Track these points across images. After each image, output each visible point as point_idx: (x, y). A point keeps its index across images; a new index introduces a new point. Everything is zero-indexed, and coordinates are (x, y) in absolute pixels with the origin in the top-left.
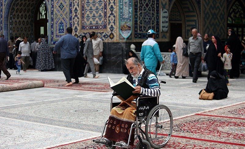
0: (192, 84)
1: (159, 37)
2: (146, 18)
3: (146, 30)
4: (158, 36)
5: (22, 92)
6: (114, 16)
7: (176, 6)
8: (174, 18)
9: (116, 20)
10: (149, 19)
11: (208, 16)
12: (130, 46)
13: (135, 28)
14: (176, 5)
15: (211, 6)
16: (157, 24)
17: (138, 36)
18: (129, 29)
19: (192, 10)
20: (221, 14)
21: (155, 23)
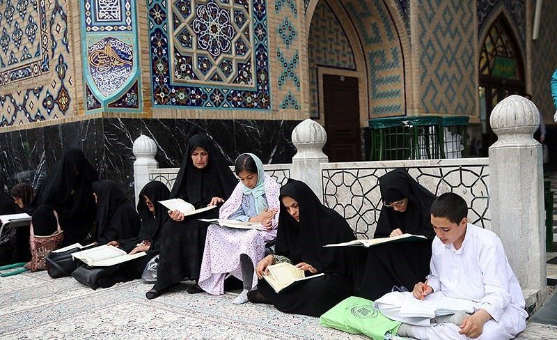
0: (456, 332)
1: (268, 103)
2: (209, 28)
3: (209, 74)
4: (264, 100)
5: (209, 258)
6: (64, 17)
7: (331, 15)
8: (344, 62)
9: (69, 32)
10: (225, 31)
11: (430, 52)
12: (209, 160)
13: (154, 62)
14: (331, 10)
15: (439, 26)
16: (258, 57)
17: (173, 96)
18: (126, 66)
19: (392, 61)
20: (466, 51)
21: (251, 52)
